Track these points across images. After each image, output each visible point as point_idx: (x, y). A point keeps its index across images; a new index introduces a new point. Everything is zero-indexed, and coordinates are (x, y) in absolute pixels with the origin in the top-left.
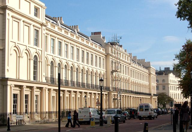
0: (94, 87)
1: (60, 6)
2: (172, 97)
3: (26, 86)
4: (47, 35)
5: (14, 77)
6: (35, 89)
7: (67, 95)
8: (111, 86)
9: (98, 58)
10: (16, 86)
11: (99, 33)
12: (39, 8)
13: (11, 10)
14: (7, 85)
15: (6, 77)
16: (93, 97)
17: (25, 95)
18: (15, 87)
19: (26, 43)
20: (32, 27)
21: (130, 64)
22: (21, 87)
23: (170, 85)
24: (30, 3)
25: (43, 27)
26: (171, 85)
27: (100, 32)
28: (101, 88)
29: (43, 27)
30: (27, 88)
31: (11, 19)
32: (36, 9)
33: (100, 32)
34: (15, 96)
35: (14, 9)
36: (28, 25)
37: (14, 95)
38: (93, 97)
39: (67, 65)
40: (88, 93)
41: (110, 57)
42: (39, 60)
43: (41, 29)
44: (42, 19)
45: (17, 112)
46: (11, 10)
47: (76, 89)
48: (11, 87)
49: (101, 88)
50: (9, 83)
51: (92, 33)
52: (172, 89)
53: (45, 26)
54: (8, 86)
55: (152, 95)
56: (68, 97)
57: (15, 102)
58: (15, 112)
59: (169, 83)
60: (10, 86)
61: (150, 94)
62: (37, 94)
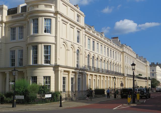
0: (129, 76)
1: (96, 17)
2: (159, 81)
3: (72, 71)
4: (85, 36)
5: (63, 64)
6: (71, 73)
7: (94, 78)
8: (125, 73)
9: (128, 58)
10: (65, 71)
11: (117, 38)
12: (80, 16)
13: (62, 15)
14: (58, 70)
15: (58, 64)
16: (119, 80)
17: (71, 78)
18: (64, 72)
19: (72, 40)
20: (75, 28)
21: (136, 59)
22: (68, 72)
23: (157, 73)
24: (67, 6)
25: (83, 29)
26: (158, 73)
27: (118, 37)
28: (134, 76)
29: (83, 30)
30: (79, 74)
31: (61, 22)
32: (78, 16)
33: (118, 37)
34: (64, 78)
35: (63, 14)
36: (72, 27)
37: (63, 77)
38: (119, 80)
39: (90, 54)
40: (111, 77)
41: (125, 53)
42: (80, 53)
43: (82, 31)
44: (82, 23)
45: (65, 90)
46: (62, 15)
47: (92, 72)
48: (61, 72)
49: (134, 76)
50: (60, 68)
51: (112, 38)
52: (160, 76)
53: (85, 29)
54: (59, 71)
55: (125, 75)
56: (49, 77)
57: (64, 83)
58: (64, 90)
59: (157, 72)
60: (60, 71)
61: (123, 75)
62: (64, 76)
